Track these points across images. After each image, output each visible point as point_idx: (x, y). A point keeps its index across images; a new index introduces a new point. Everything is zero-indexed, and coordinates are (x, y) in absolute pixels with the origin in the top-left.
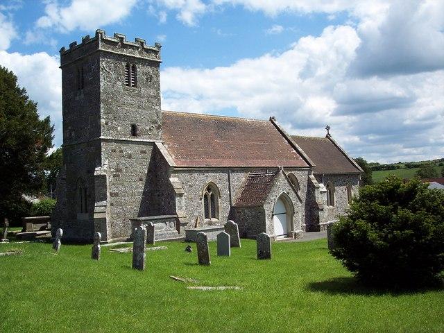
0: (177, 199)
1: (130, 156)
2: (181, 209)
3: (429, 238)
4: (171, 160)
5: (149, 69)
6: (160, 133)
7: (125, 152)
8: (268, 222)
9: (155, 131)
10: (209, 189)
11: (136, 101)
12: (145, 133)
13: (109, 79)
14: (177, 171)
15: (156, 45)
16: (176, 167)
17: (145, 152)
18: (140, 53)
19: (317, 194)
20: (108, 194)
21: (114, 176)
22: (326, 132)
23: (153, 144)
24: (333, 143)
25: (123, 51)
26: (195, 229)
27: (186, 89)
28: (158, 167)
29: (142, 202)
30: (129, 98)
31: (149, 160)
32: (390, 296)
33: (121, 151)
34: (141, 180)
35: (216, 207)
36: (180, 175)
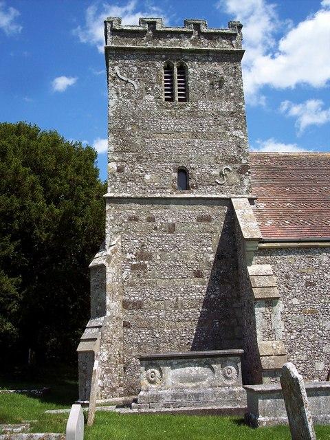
0: (259, 312)
1: (172, 229)
2: (270, 334)
4: (250, 227)
5: (218, 68)
6: (246, 182)
7: (159, 222)
9: (234, 177)
11: (186, 125)
12: (210, 182)
14: (265, 250)
15: (232, 26)
16: (260, 241)
17: (208, 219)
18: (193, 42)
21: (134, 268)
23: (228, 202)
25: (155, 44)
26: (304, 393)
28: (232, 250)
29: (203, 322)
30: (172, 122)
31: (216, 237)
32: (314, 101)
33: (151, 219)
34: (198, 274)
36: (279, 259)
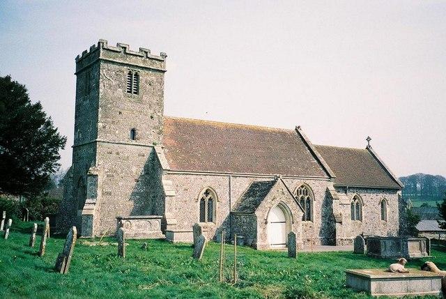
3: (7, 150)
8: (260, 230)
10: (207, 193)
13: (110, 83)
18: (144, 61)
19: (335, 204)
20: (99, 192)
22: (366, 143)
24: (373, 155)
27: (188, 96)
28: (152, 169)
30: (129, 104)
33: (118, 154)
35: (214, 211)
